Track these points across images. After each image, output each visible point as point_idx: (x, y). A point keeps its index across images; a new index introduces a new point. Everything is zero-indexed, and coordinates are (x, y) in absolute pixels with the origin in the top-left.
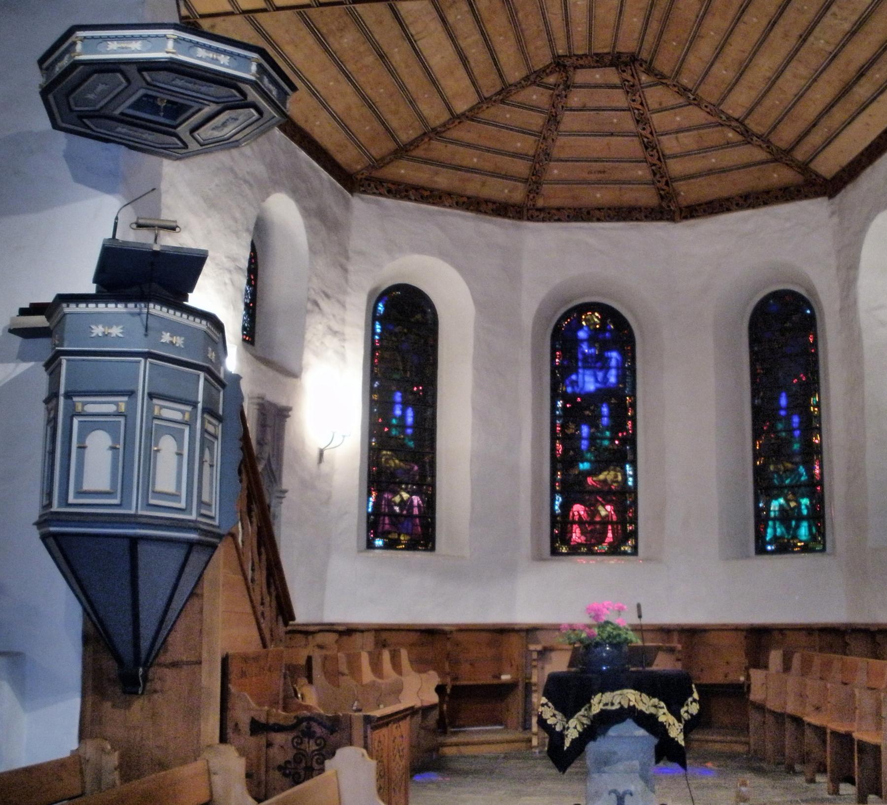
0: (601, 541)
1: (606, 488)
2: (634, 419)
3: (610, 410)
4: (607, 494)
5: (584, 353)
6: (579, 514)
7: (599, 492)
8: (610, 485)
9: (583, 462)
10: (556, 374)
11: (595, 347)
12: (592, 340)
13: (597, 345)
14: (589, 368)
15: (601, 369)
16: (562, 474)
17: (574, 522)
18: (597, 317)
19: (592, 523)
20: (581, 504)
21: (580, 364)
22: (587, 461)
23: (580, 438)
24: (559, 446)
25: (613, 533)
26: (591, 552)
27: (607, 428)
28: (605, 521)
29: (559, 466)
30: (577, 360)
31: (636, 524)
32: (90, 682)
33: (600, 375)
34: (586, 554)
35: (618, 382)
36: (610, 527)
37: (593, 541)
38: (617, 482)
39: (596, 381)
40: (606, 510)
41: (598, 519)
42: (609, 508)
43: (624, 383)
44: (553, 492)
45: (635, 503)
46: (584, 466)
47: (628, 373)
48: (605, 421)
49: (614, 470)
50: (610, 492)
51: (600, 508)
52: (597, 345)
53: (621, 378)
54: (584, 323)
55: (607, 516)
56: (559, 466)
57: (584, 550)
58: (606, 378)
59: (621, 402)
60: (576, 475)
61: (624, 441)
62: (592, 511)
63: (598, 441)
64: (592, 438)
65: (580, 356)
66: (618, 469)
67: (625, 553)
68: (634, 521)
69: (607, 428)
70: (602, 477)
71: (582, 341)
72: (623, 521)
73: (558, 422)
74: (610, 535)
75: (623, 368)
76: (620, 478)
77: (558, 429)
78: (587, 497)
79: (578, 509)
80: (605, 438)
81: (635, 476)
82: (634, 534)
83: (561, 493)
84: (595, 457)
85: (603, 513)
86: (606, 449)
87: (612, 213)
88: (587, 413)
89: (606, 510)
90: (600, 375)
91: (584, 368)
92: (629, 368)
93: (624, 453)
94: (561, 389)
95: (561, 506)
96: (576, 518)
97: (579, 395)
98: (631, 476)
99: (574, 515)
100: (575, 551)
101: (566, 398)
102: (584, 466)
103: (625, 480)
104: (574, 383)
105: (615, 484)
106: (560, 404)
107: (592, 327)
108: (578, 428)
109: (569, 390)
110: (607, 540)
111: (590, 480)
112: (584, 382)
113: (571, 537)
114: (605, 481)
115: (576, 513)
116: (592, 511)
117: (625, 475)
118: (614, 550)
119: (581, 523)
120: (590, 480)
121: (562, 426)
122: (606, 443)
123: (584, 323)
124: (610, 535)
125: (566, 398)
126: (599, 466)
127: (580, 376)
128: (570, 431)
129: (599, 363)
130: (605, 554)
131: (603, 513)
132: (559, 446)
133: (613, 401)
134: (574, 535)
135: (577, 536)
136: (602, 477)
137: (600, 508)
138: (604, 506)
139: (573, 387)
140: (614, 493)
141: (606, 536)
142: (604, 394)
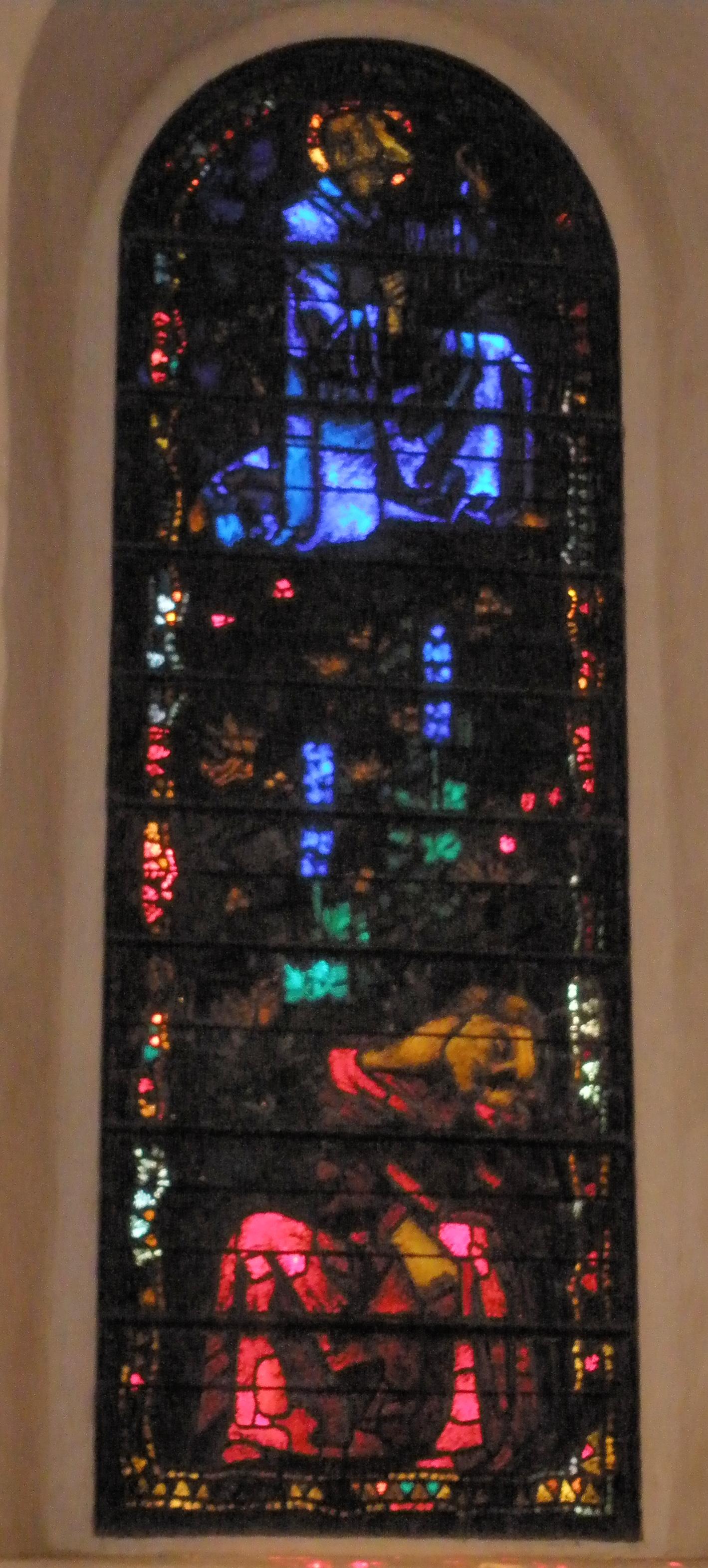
0: (408, 1449)
1: (442, 1120)
2: (609, 715)
3: (466, 655)
4: (449, 1153)
5: (312, 321)
6: (277, 1273)
7: (394, 1137)
8: (470, 1099)
9: (304, 956)
10: (147, 437)
11: (379, 298)
12: (360, 252)
13: (392, 284)
14: (343, 413)
15: (414, 421)
16: (173, 1026)
17: (244, 1324)
18: (393, 129)
19: (351, 1327)
20: (290, 1214)
21: (294, 388)
22: (332, 952)
23: (294, 816)
24: (155, 850)
25: (485, 1395)
26: (344, 1513)
27: (454, 759)
28: (433, 1330)
29: (159, 972)
30: (275, 368)
31: (626, 1339)
32: (470, 1214)
33: (412, 455)
34: (320, 1523)
35: (511, 495)
36: (465, 1358)
37: (363, 1444)
38: (505, 1079)
39: (387, 486)
40: (437, 1251)
41: (389, 1305)
42: (457, 1236)
43: (550, 503)
44: (119, 1136)
45: (616, 1214)
46: (317, 981)
47: (576, 445)
48: (438, 720)
49: (489, 1009)
50: (463, 1142)
51: (409, 1238)
52: (392, 284)
53: (534, 471)
54: (317, 156)
55: (444, 1287)
56: (159, 972)
57: (303, 1495)
58: (443, 466)
59: (531, 604)
60: (255, 1033)
61: (545, 838)
62: (356, 1254)
63: (398, 836)
64: (362, 819)
65: (295, 344)
66: (517, 1002)
67: (557, 1522)
68: (616, 1317)
69: (454, 759)
70: (416, 1048)
71: (310, 253)
72: (546, 1325)
73: (158, 715)
74: (466, 1406)
75: (548, 424)
76: (525, 1058)
77: (157, 752)
78: (326, 1170)
79: (271, 1239)
80: (442, 822)
81: (616, 1049)
82: (615, 1402)
83: (170, 1139)
84: (378, 931)
85: (426, 1269)
86: (444, 877)
87: (620, 1056)
88: (332, 666)
89: (437, 1251)
90: (412, 455)
91: (318, 409)
92: (575, 423)
93: (560, 921)
94: (177, 521)
95: (165, 1219)
96: (260, 1294)
97: (291, 564)
98: (590, 1047)
99: (242, 1273)
100: (246, 1502)
101: (207, 572)
102: (317, 981)
103: (559, 1076)
104: (259, 496)
105: (499, 1096)
106: (167, 607)
107: (363, 184)
108: (280, 749)
109: (229, 529)
110: (451, 1438)
111: (342, 1065)
112: (318, 489)
113: (228, 1415)
114: (435, 1074)
115: (257, 1266)
116: (356, 1254)
117: (555, 1036)
118: (492, 1502)
119: (288, 1326)
120: (342, 1065)
121: (175, 737)
122: (444, 847)
123: (317, 156)
124: (466, 1406)
125: (207, 572)
126: (406, 973)
127: (296, 454)
128: (227, 771)
129: (401, 387)
130: (440, 1522)
131: (426, 1269)
132: (155, 850)
133: (488, 603)
134: (245, 1401)
135: (258, 1403)
136: (416, 1048)
137: (409, 1238)
138: (429, 1224)
139: (249, 517)
140: (495, 1147)
141: (441, 1419)
142: (426, 561)
